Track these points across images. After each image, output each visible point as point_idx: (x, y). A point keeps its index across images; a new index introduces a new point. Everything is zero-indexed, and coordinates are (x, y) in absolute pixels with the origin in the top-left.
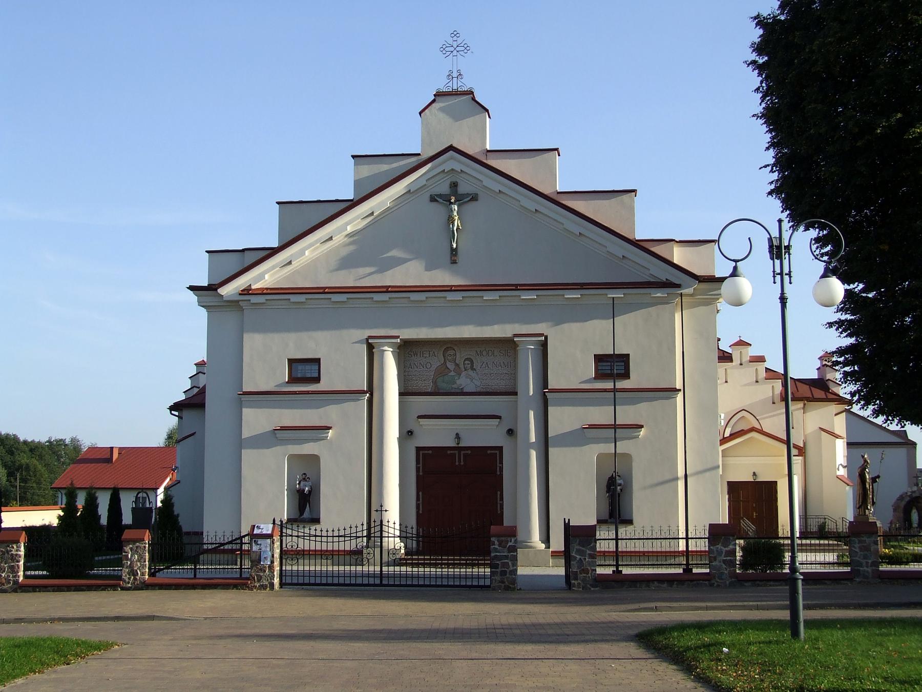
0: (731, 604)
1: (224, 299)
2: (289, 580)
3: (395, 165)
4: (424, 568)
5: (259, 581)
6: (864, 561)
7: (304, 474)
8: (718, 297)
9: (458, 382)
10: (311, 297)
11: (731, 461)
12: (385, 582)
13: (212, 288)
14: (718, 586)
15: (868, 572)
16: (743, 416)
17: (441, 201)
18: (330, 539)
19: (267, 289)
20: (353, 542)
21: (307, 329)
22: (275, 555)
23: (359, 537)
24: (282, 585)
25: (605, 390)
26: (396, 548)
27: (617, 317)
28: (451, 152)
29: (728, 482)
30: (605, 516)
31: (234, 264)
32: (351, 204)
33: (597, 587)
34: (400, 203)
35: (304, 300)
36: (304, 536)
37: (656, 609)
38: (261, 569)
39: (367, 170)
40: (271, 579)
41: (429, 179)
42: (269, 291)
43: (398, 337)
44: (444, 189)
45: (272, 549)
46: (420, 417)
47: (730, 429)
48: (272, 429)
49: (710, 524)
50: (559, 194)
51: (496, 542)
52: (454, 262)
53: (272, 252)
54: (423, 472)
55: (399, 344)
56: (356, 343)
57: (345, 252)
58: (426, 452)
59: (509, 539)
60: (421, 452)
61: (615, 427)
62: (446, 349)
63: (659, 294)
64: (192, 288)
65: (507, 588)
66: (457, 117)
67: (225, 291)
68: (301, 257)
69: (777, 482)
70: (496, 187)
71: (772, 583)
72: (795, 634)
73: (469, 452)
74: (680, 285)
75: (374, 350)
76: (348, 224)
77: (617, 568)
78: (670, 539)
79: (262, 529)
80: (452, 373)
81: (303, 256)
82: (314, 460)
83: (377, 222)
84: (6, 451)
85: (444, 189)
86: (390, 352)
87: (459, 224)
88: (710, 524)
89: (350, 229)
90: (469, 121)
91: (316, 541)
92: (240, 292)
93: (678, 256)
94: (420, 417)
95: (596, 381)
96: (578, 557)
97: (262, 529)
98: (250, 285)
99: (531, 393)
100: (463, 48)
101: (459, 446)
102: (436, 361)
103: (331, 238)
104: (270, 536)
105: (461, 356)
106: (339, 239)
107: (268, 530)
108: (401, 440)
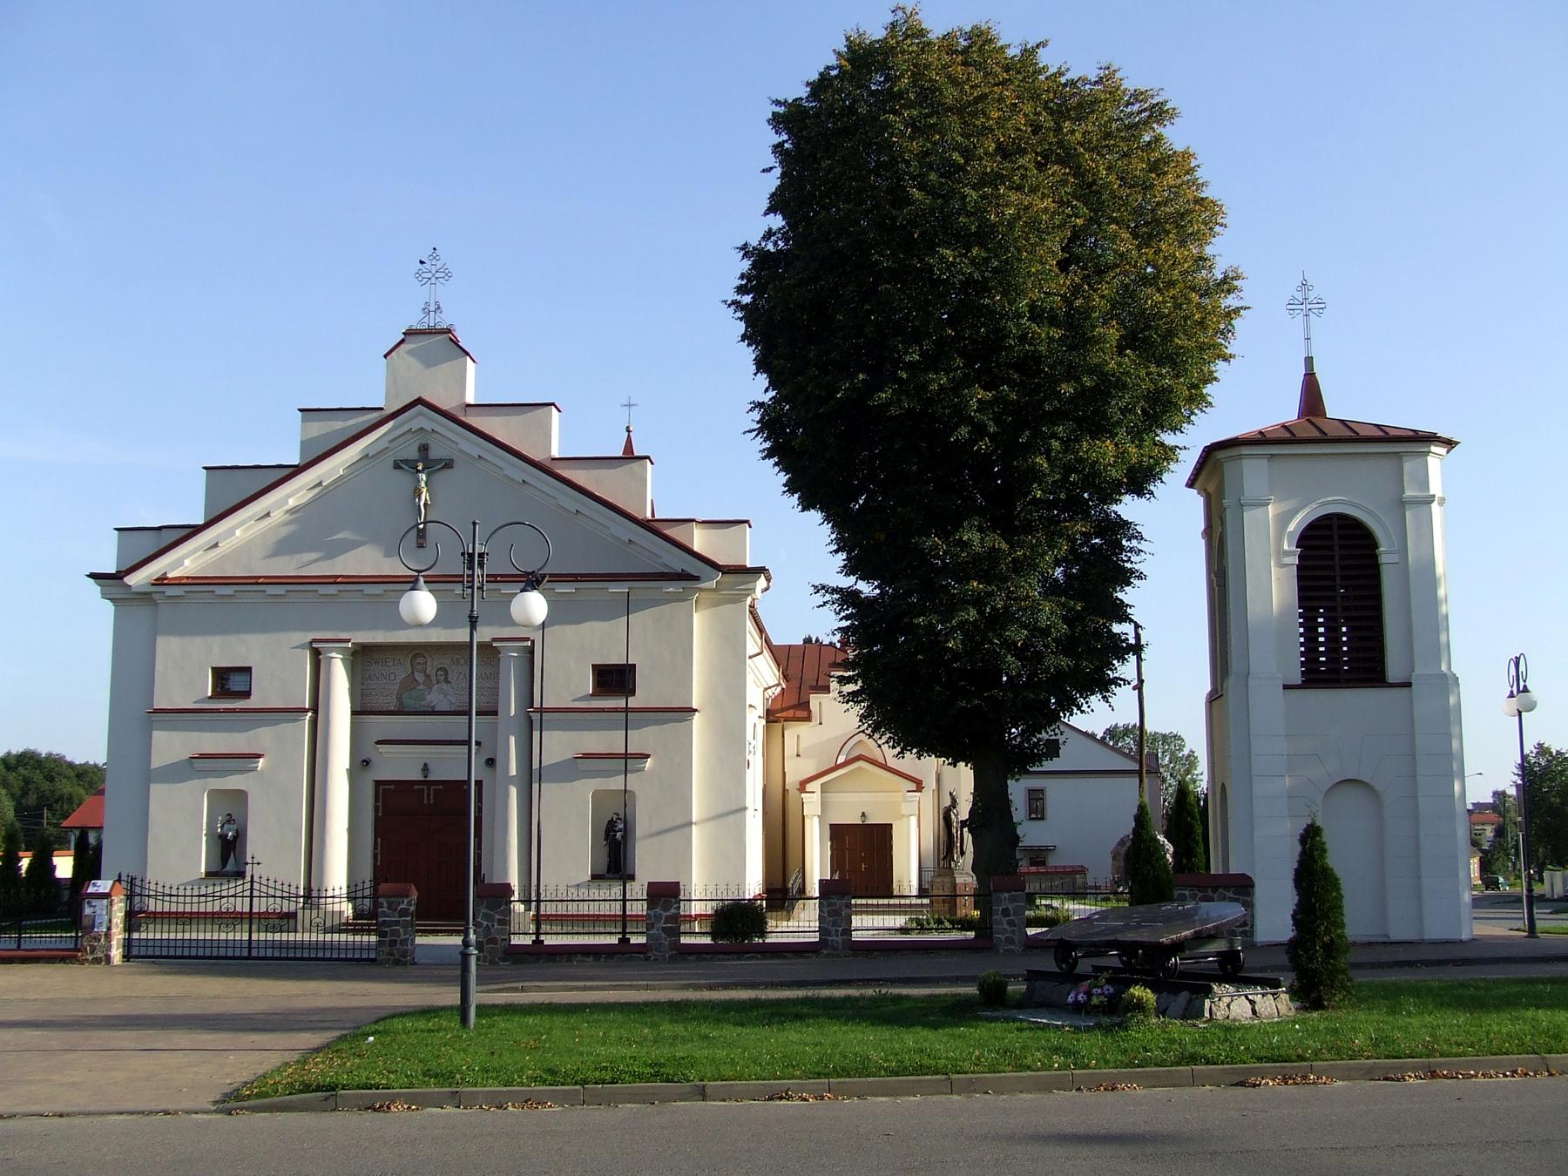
0: (615, 983)
1: (133, 590)
2: (135, 951)
3: (351, 422)
4: (369, 935)
5: (92, 953)
6: (833, 929)
7: (229, 815)
8: (749, 592)
9: (429, 698)
11: (833, 797)
12: (254, 953)
13: (118, 576)
14: (655, 960)
15: (837, 942)
17: (407, 468)
18: (188, 900)
19: (188, 578)
20: (217, 902)
21: (238, 631)
22: (114, 921)
23: (224, 897)
24: (127, 957)
25: (616, 710)
26: (269, 911)
28: (420, 406)
29: (831, 825)
30: (603, 869)
31: (148, 544)
32: (297, 470)
33: (506, 961)
35: (182, 594)
36: (156, 896)
37: (523, 990)
38: (95, 938)
39: (319, 428)
40: (107, 950)
41: (393, 440)
42: (190, 581)
43: (348, 641)
44: (412, 452)
45: (110, 913)
46: (379, 742)
47: (844, 757)
48: (187, 757)
49: (649, 883)
50: (554, 461)
51: (385, 904)
52: (421, 546)
53: (195, 530)
54: (382, 812)
55: (352, 650)
56: (296, 647)
57: (285, 531)
58: (387, 787)
59: (401, 900)
60: (381, 787)
61: (626, 756)
62: (415, 656)
63: (671, 588)
64: (93, 576)
65: (397, 963)
66: (429, 361)
67: (134, 580)
68: (230, 537)
69: (891, 825)
70: (475, 452)
71: (721, 957)
72: (464, 1020)
73: (441, 787)
74: (698, 577)
75: (320, 657)
76: (289, 496)
77: (624, 936)
78: (556, 901)
79: (99, 886)
80: (422, 687)
81: (232, 536)
82: (240, 796)
83: (325, 493)
84: (44, 777)
85: (412, 452)
87: (428, 498)
88: (649, 883)
89: (292, 503)
90: (446, 368)
91: (177, 903)
92: (154, 582)
93: (700, 541)
94: (379, 742)
95: (593, 698)
96: (486, 923)
97: (99, 886)
98: (166, 573)
99: (513, 713)
100: (443, 275)
102: (401, 671)
103: (268, 515)
104: (107, 896)
105: (432, 664)
106: (278, 516)
107: (105, 888)
108: (353, 774)
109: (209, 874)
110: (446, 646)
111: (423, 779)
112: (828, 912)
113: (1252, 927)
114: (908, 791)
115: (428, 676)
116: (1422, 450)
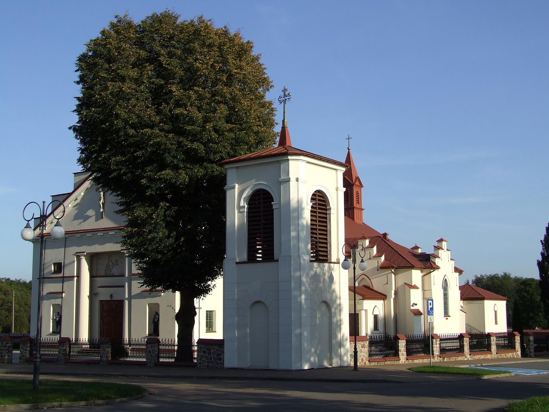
10: (47, 237)
15: (104, 360)
16: (363, 278)
19: (47, 233)
27: (67, 247)
34: (88, 192)
73: (117, 302)
82: (157, 305)
86: (84, 259)
101: (112, 299)
109: (53, 332)
110: (105, 253)
111: (110, 299)
112: (103, 349)
113: (224, 361)
114: (360, 300)
115: (113, 263)
116: (285, 159)
